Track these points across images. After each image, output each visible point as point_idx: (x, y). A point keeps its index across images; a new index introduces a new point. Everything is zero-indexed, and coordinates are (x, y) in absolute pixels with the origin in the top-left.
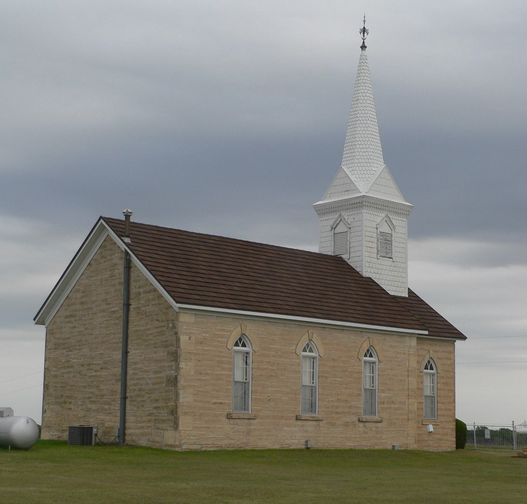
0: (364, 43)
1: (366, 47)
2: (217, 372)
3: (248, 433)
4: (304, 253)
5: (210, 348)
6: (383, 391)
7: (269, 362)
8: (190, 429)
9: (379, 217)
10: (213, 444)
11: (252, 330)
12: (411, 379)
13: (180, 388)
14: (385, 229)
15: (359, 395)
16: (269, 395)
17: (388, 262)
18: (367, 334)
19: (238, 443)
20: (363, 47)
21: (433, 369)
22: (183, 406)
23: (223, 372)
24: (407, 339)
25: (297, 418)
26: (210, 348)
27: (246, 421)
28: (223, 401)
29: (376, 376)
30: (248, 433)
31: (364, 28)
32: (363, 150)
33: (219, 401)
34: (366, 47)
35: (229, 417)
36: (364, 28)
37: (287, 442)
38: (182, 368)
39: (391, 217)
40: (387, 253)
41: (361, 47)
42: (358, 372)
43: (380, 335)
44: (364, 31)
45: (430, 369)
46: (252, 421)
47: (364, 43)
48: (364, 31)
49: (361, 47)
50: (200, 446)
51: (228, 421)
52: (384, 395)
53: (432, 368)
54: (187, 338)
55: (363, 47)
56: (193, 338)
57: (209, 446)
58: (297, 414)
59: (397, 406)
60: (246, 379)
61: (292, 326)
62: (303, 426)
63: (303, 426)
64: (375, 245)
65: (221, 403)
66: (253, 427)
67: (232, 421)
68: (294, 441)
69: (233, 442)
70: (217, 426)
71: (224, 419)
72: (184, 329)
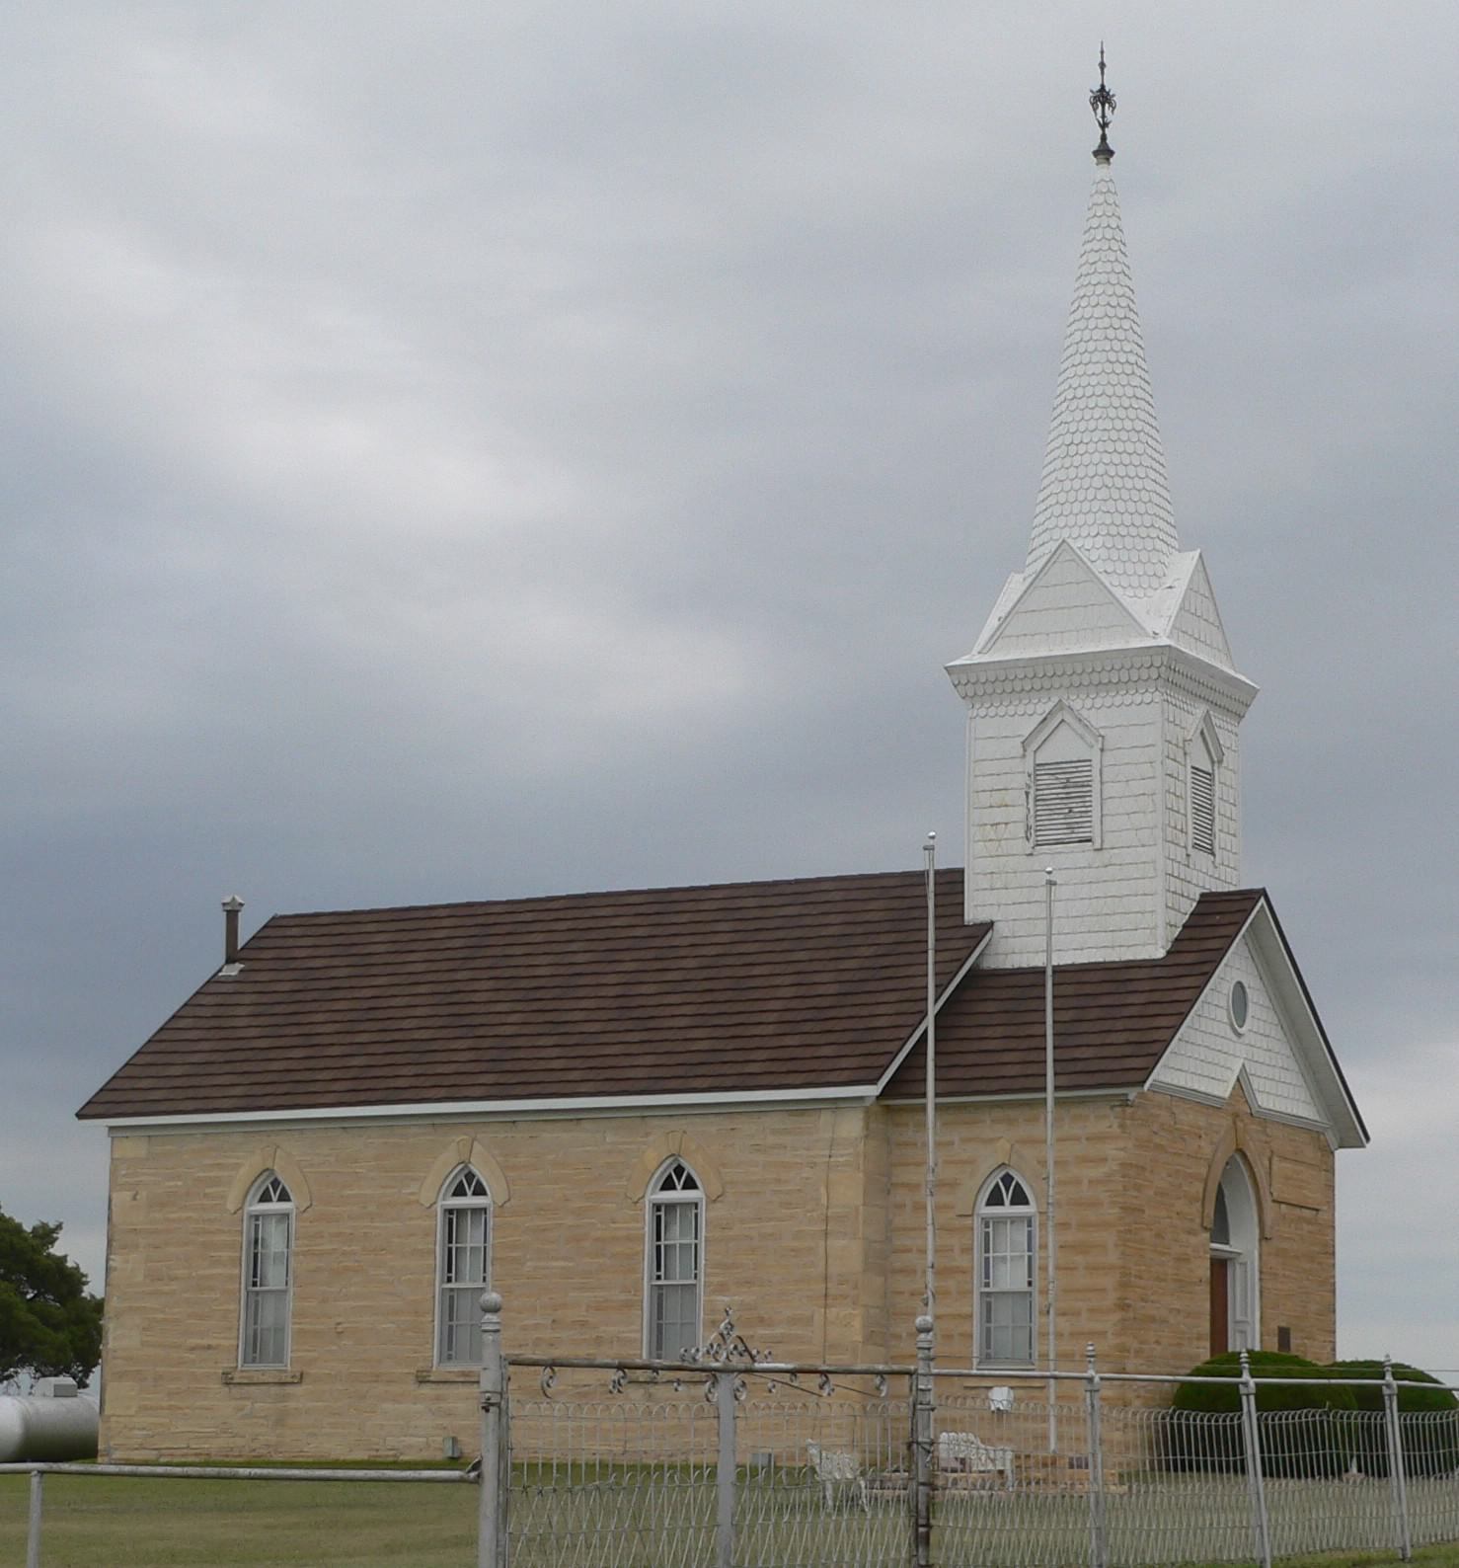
0: (1104, 138)
1: (1112, 153)
2: (201, 1272)
3: (280, 1421)
4: (893, 882)
5: (184, 1215)
6: (722, 1289)
7: (339, 1234)
8: (132, 1412)
9: (1022, 717)
10: (188, 1447)
11: (291, 1159)
12: (837, 1244)
13: (111, 1315)
14: (1064, 747)
15: (628, 1305)
16: (340, 1320)
17: (1081, 855)
18: (665, 1122)
19: (254, 1445)
20: (1104, 152)
21: (1026, 1202)
22: (114, 1358)
23: (219, 1271)
24: (826, 1118)
25: (422, 1380)
26: (184, 1215)
27: (274, 1390)
28: (213, 1342)
29: (701, 1242)
30: (280, 1421)
31: (1103, 87)
32: (1129, 484)
33: (205, 1342)
34: (1112, 153)
35: (228, 1380)
36: (1103, 87)
37: (391, 1442)
38: (115, 1269)
39: (1077, 705)
40: (1070, 827)
41: (1096, 153)
42: (629, 1239)
43: (712, 1119)
44: (1102, 97)
45: (1013, 1203)
46: (289, 1389)
47: (1104, 138)
48: (1102, 97)
49: (1096, 153)
50: (154, 1452)
51: (227, 1389)
52: (726, 1299)
53: (1020, 1198)
54: (127, 1195)
55: (1104, 152)
56: (143, 1194)
57: (179, 1452)
58: (421, 1365)
59: (779, 1331)
60: (1030, 1283)
61: (414, 1130)
62: (438, 1398)
63: (438, 1398)
64: (1018, 813)
65: (209, 1347)
66: (292, 1405)
67: (235, 1391)
68: (414, 1440)
69: (239, 1442)
70: (197, 1404)
71: (216, 1386)
72: (124, 1176)
